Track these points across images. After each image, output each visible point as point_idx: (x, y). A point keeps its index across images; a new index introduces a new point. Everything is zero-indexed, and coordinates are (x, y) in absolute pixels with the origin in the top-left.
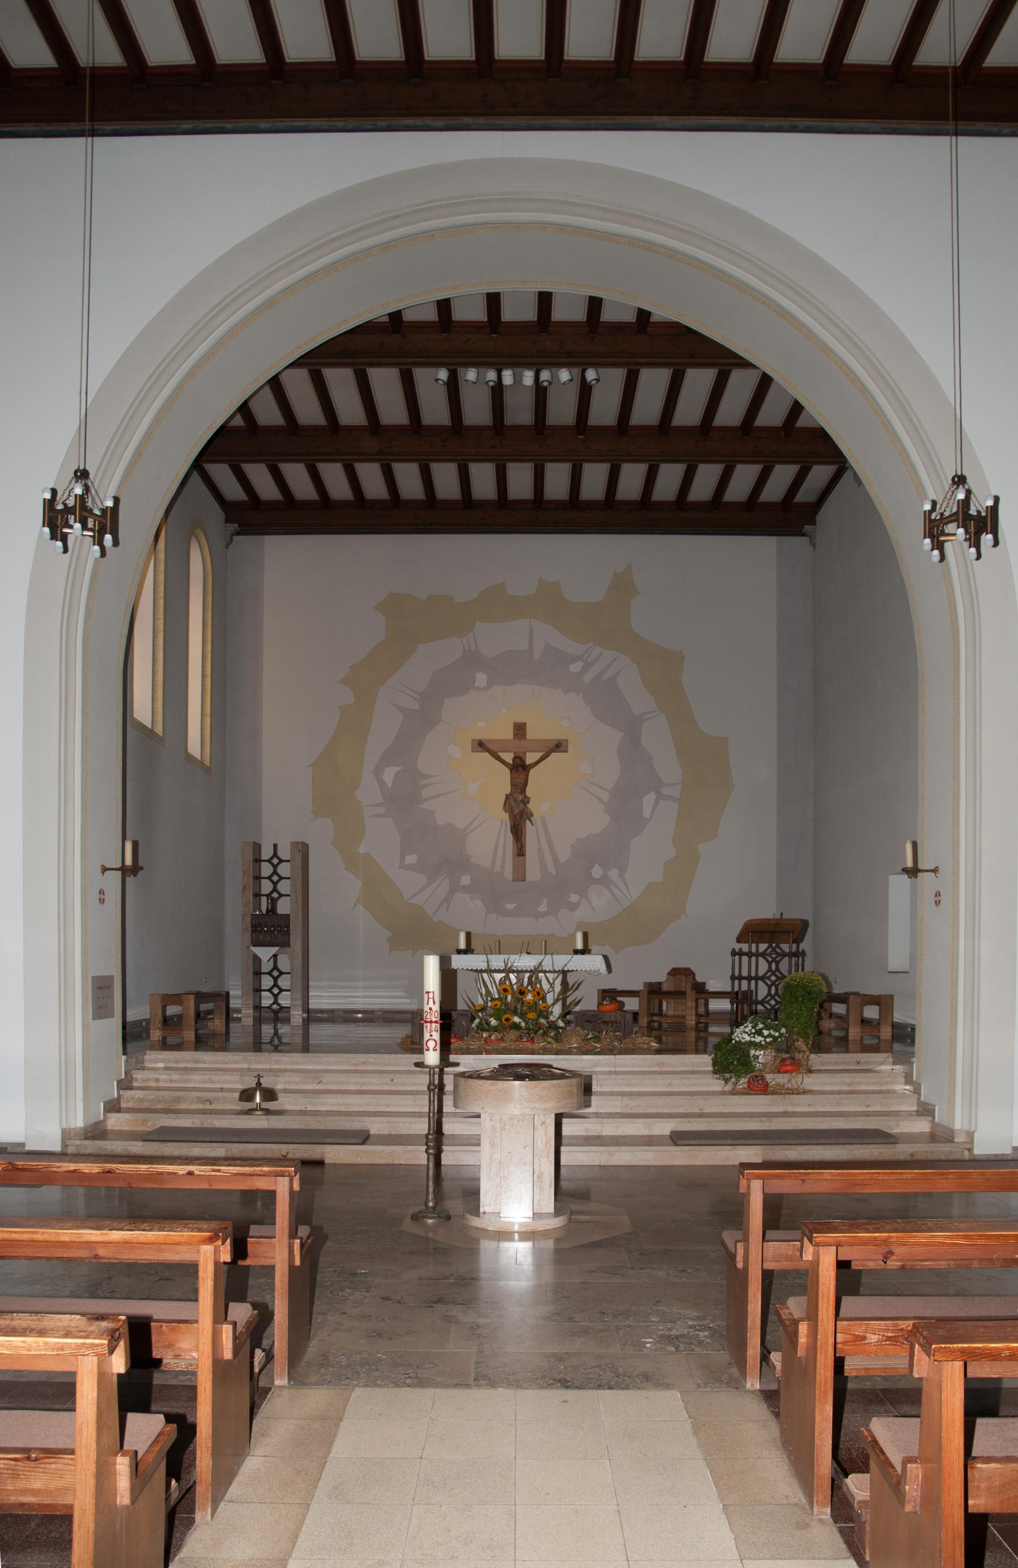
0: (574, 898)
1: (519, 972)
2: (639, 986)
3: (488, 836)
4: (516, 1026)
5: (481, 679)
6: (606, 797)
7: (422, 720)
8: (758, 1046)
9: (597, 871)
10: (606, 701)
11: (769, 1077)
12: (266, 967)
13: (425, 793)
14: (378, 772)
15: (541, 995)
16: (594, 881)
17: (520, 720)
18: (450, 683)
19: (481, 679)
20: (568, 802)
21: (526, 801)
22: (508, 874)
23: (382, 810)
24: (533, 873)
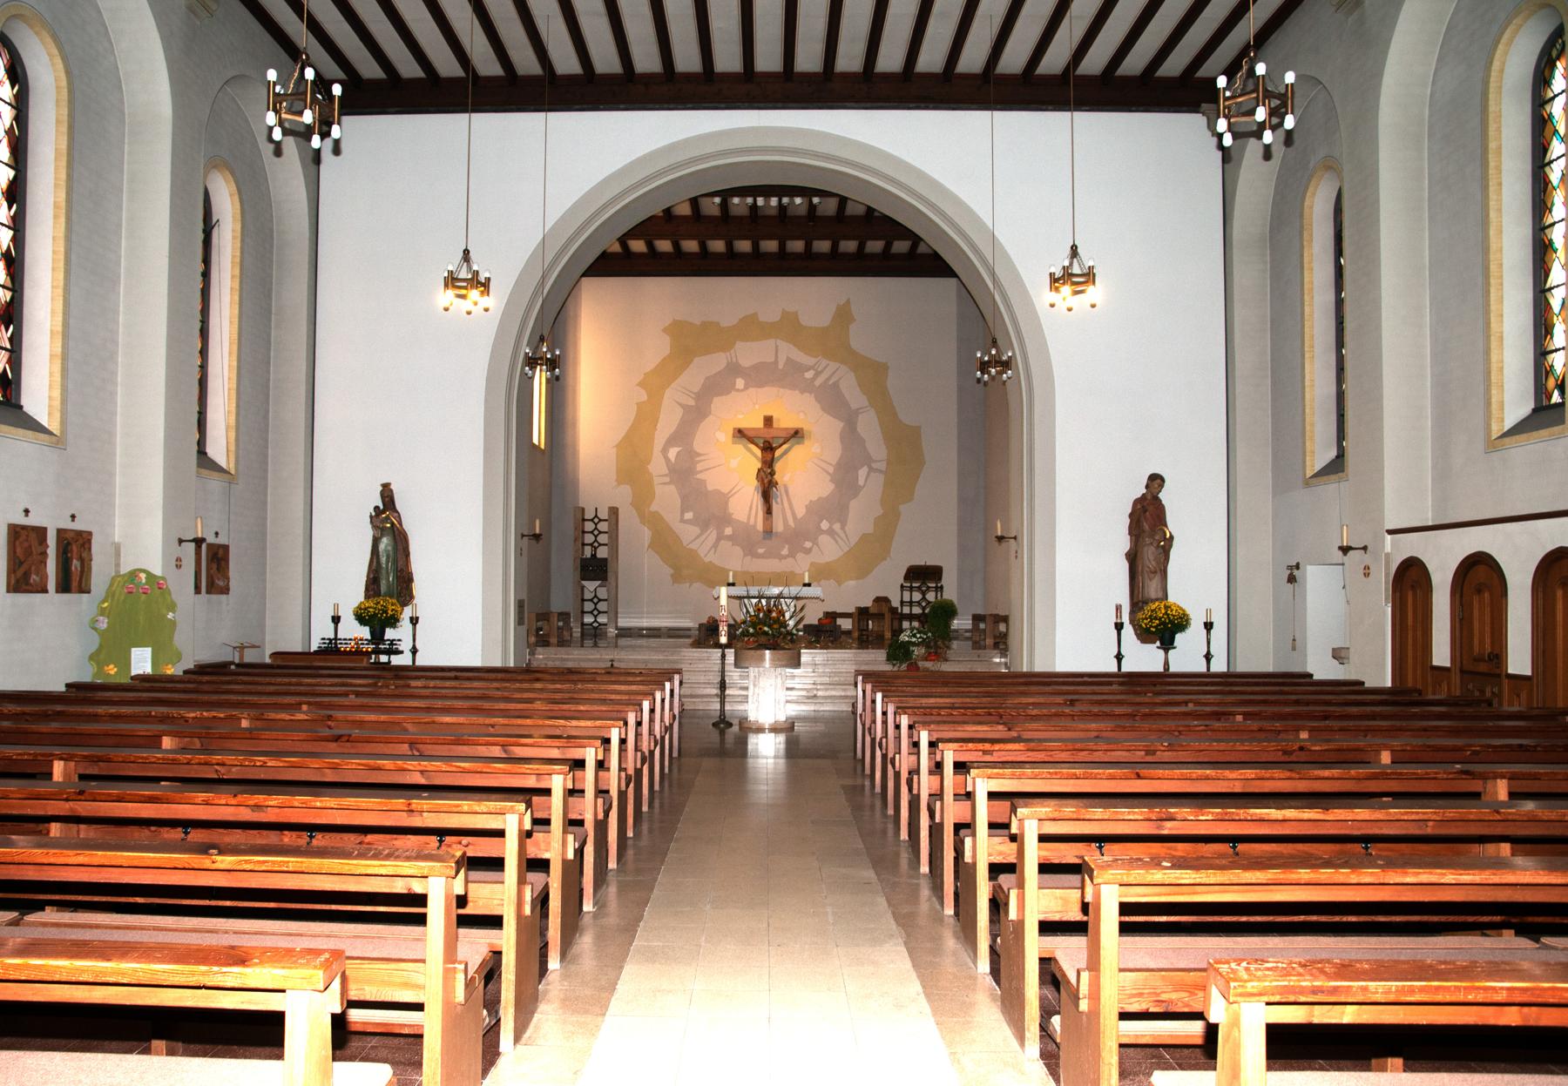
0: (808, 545)
1: (768, 598)
2: (852, 610)
3: (745, 502)
4: (766, 633)
5: (740, 383)
6: (831, 470)
7: (696, 413)
8: (914, 644)
9: (825, 525)
10: (832, 401)
11: (920, 664)
12: (588, 596)
13: (699, 467)
14: (665, 451)
15: (782, 613)
16: (823, 532)
17: (769, 414)
18: (716, 386)
19: (740, 383)
20: (804, 476)
21: (772, 474)
22: (760, 527)
23: (667, 479)
24: (778, 526)
